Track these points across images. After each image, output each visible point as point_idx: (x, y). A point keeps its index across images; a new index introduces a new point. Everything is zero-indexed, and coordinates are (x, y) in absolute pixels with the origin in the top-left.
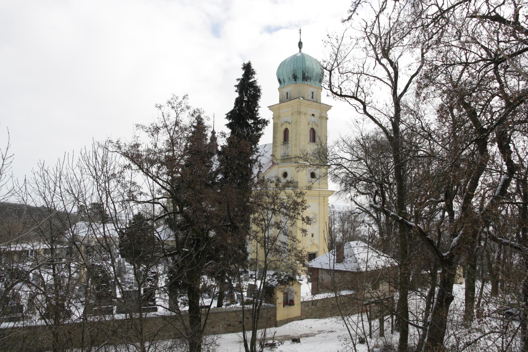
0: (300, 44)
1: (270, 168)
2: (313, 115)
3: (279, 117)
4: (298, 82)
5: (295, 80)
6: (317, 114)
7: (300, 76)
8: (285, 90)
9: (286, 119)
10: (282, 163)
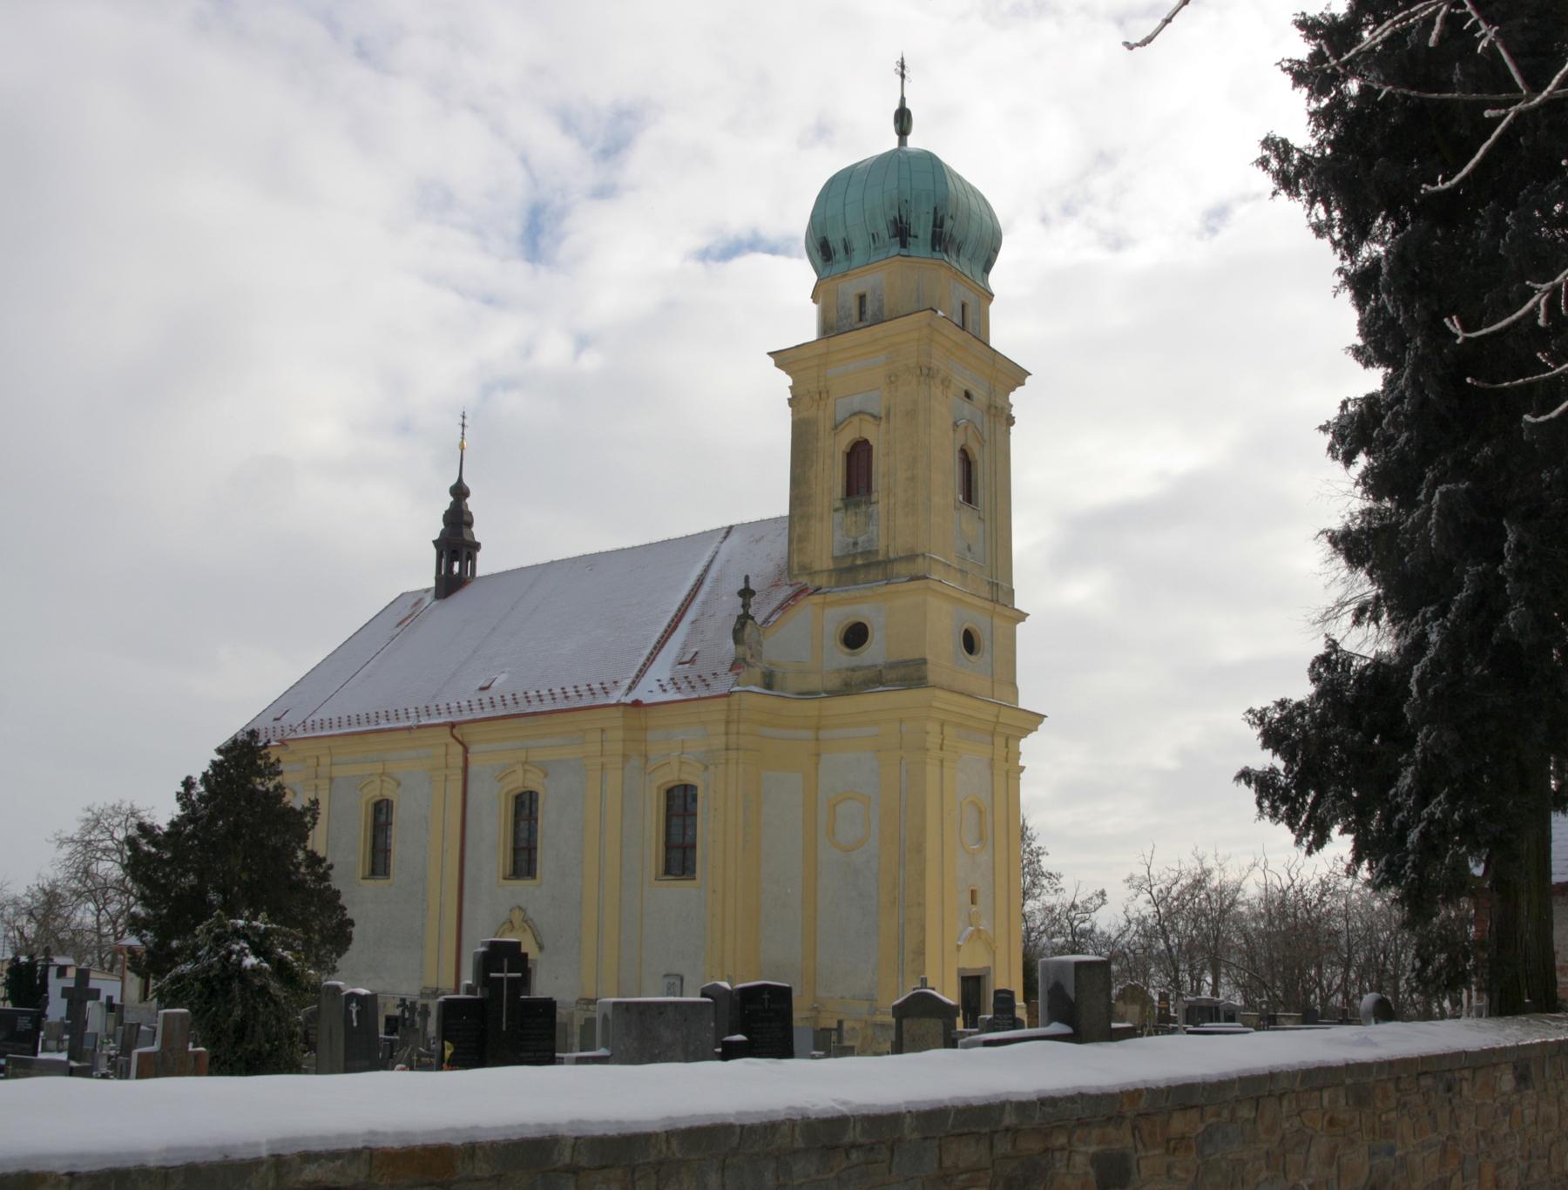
0: (903, 120)
1: (783, 607)
2: (968, 395)
3: (822, 394)
4: (913, 250)
5: (904, 245)
6: (979, 394)
7: (922, 228)
8: (851, 287)
9: (857, 402)
10: (838, 584)
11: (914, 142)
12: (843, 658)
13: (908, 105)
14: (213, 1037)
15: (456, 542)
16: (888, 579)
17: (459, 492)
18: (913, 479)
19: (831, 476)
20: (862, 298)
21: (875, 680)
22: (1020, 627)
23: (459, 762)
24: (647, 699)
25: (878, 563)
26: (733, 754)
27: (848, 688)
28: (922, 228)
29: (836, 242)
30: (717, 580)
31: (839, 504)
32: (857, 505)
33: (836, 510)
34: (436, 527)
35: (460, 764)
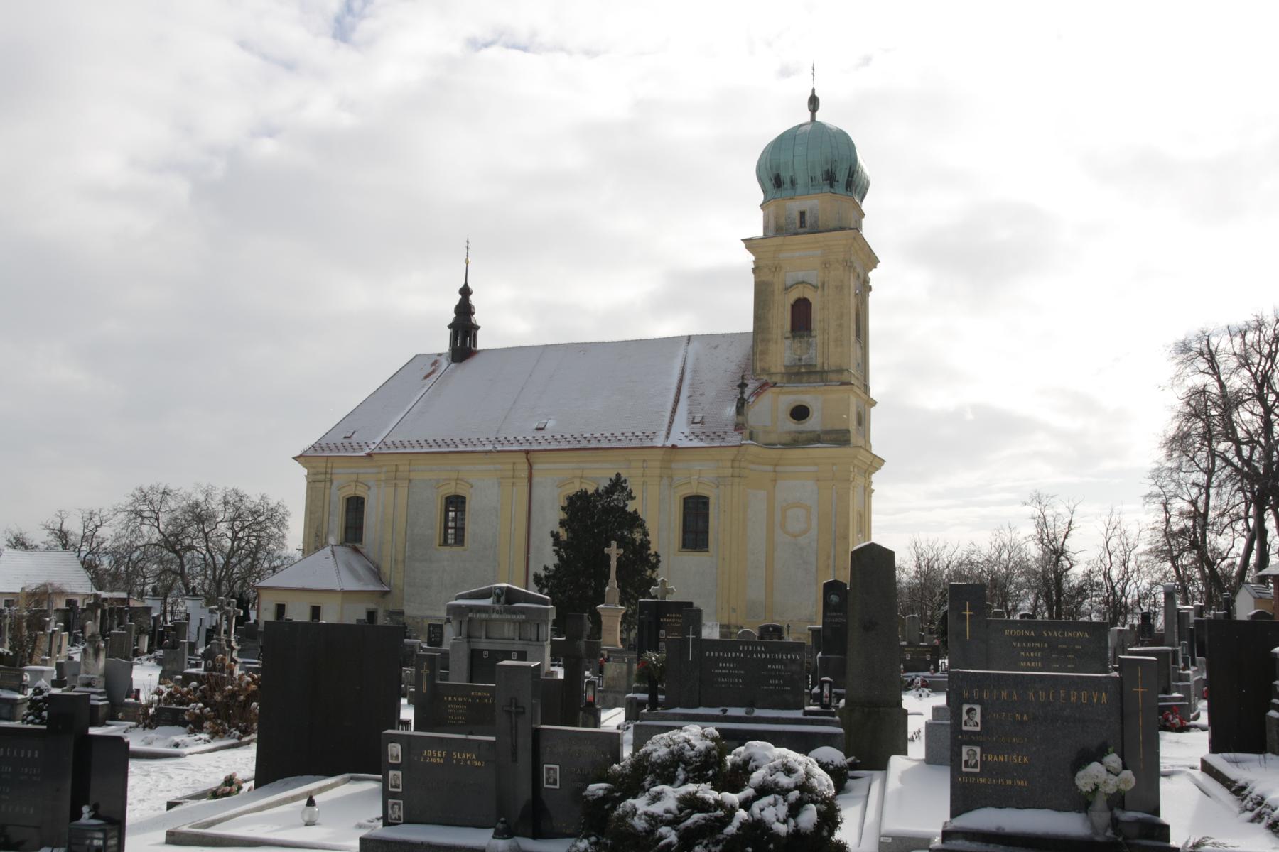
0: (814, 102)
3: (776, 268)
5: (832, 186)
7: (842, 177)
8: (794, 206)
9: (800, 276)
10: (789, 382)
11: (819, 117)
12: (792, 425)
13: (817, 94)
15: (464, 324)
16: (826, 382)
17: (466, 292)
18: (841, 325)
19: (782, 318)
20: (802, 214)
21: (816, 439)
22: (873, 409)
23: (525, 474)
24: (680, 444)
25: (816, 372)
26: (737, 480)
27: (796, 442)
28: (842, 177)
29: (785, 176)
30: (694, 371)
31: (788, 335)
32: (802, 337)
34: (451, 316)
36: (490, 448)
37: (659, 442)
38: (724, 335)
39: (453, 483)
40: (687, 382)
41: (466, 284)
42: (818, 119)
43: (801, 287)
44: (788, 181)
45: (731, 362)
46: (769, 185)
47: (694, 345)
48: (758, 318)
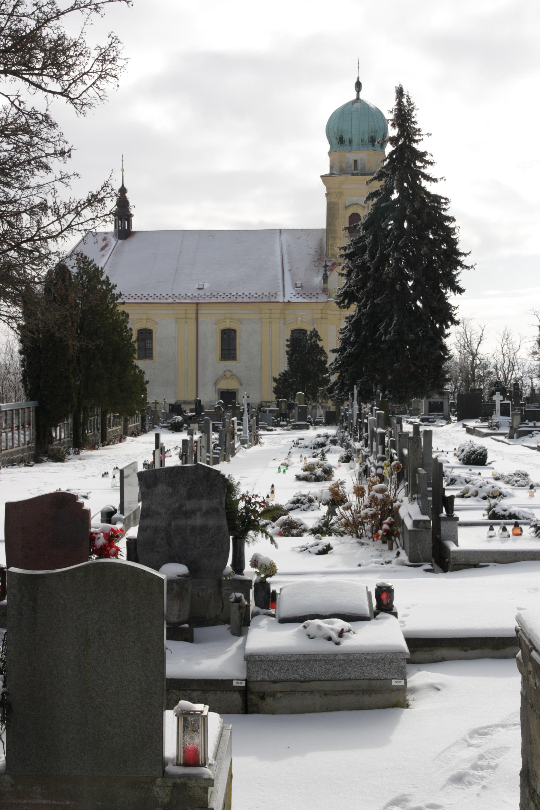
3: (341, 194)
8: (351, 156)
9: (354, 200)
13: (360, 80)
14: (439, 203)
20: (356, 161)
26: (324, 320)
29: (346, 138)
30: (289, 253)
33: (346, 237)
35: (194, 316)
36: (171, 300)
37: (280, 299)
38: (302, 230)
39: (144, 322)
40: (286, 261)
41: (123, 185)
42: (361, 97)
43: (355, 207)
44: (348, 141)
45: (309, 249)
46: (335, 141)
47: (284, 237)
48: (329, 223)
